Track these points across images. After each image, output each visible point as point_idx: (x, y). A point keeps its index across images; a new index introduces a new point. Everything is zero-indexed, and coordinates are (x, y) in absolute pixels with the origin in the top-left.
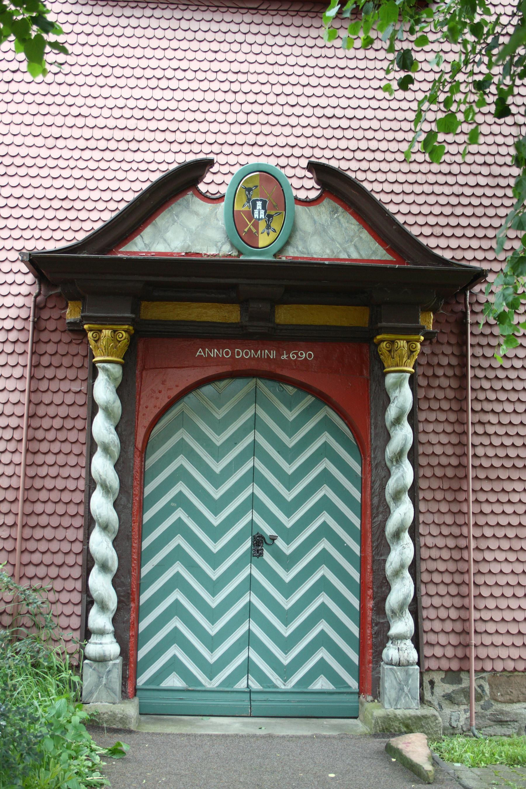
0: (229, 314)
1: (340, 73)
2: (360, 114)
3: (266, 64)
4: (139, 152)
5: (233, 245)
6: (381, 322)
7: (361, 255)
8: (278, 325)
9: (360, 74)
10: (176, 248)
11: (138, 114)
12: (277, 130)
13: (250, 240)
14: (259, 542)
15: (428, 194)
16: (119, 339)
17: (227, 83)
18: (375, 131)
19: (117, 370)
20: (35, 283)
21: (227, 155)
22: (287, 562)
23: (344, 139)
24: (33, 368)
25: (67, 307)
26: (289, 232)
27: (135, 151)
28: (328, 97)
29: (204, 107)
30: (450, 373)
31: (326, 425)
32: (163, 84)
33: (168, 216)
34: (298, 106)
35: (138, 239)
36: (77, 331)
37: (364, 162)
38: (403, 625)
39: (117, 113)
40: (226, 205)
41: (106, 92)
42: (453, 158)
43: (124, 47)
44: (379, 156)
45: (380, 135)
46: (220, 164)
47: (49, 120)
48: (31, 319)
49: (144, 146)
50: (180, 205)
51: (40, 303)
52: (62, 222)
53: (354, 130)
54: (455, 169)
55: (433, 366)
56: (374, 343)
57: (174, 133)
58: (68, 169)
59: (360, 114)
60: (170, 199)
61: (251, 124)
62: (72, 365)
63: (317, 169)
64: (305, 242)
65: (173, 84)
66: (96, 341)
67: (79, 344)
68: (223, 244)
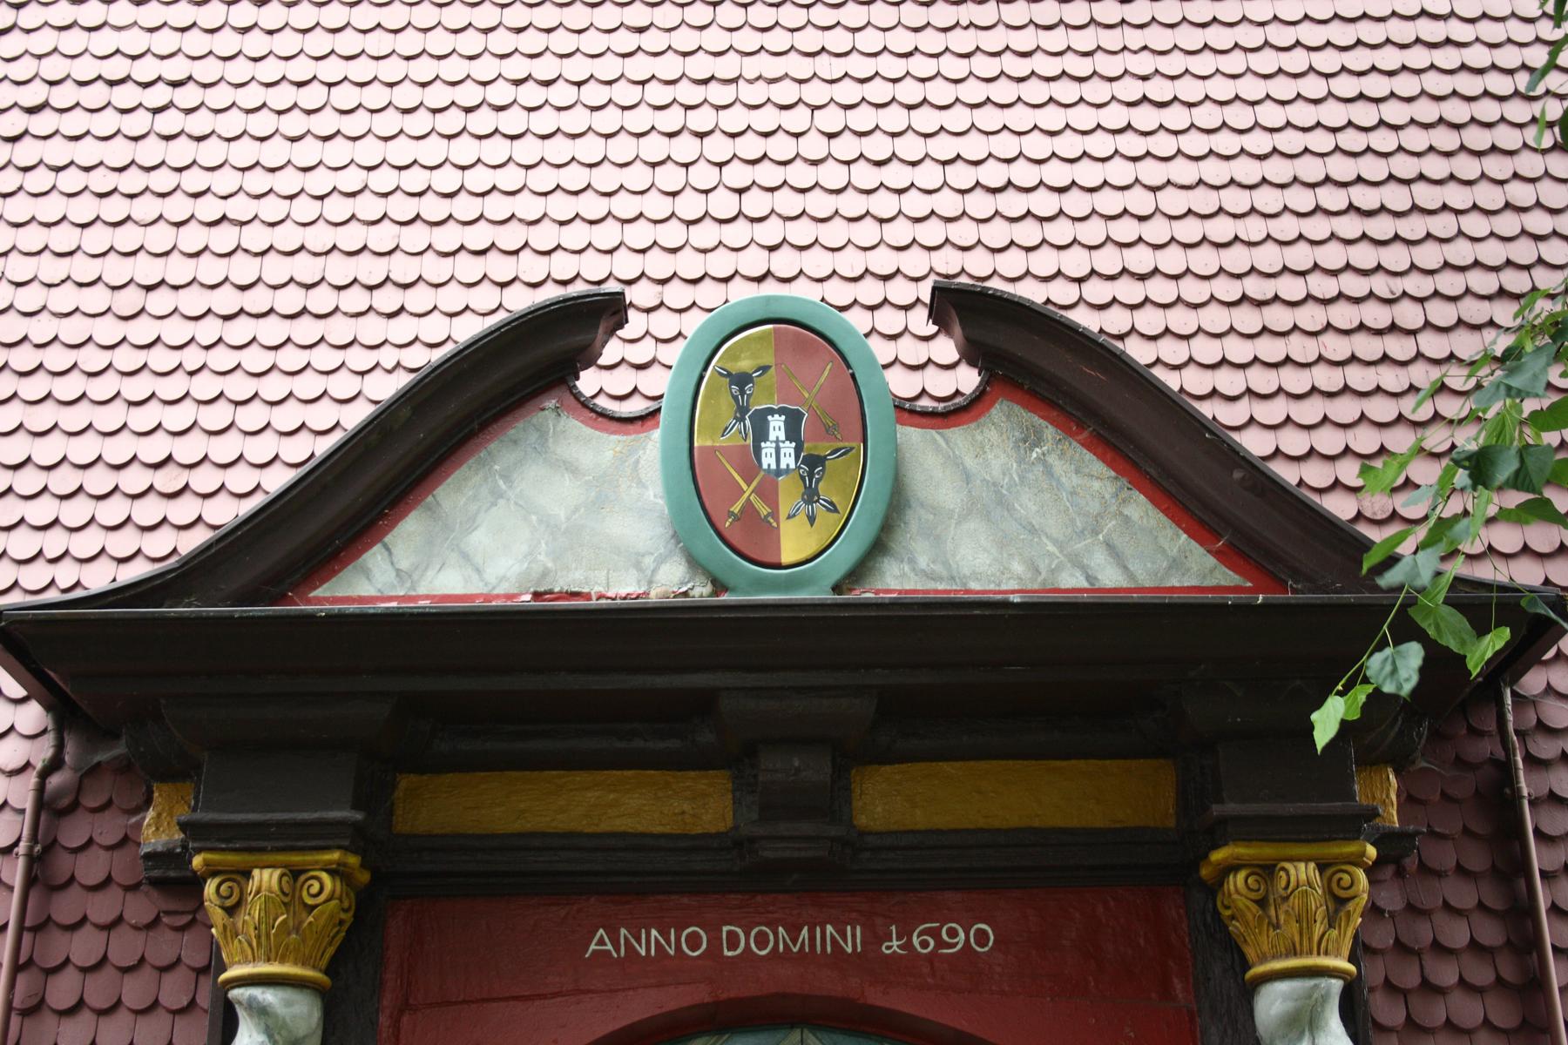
0: (693, 805)
1: (1019, 67)
2: (1088, 174)
3: (793, 54)
4: (403, 317)
5: (694, 564)
6: (1220, 801)
7: (1132, 576)
8: (863, 834)
9: (1080, 67)
10: (503, 578)
11: (402, 208)
12: (834, 233)
13: (751, 539)
15: (1330, 395)
16: (310, 901)
17: (676, 111)
18: (1142, 219)
20: (44, 732)
21: (680, 311)
23: (1045, 248)
24: (15, 1020)
25: (148, 802)
26: (880, 509)
27: (391, 316)
28: (987, 133)
29: (606, 178)
30: (1482, 974)
32: (482, 121)
33: (477, 479)
34: (895, 164)
35: (375, 558)
36: (173, 881)
37: (1115, 309)
39: (337, 208)
40: (665, 438)
41: (307, 152)
42: (1399, 285)
43: (365, 32)
44: (1161, 290)
45: (1157, 231)
46: (657, 340)
47: (127, 238)
48: (22, 848)
49: (418, 299)
50: (515, 442)
51: (60, 792)
52: (148, 536)
53: (1074, 219)
54: (1409, 315)
55: (1418, 954)
56: (1202, 883)
57: (513, 259)
58: (180, 375)
59: (1088, 174)
60: (485, 426)
61: (753, 220)
62: (155, 1004)
63: (962, 307)
64: (938, 540)
65: (512, 121)
66: (231, 911)
67: (181, 929)
68: (661, 561)
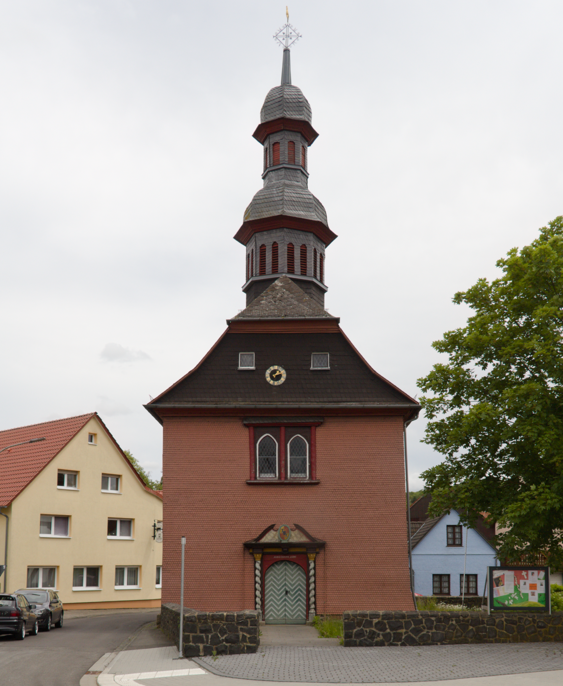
0: (279, 550)
14: (287, 592)
19: (259, 562)
22: (292, 596)
31: (299, 569)
38: (313, 592)
